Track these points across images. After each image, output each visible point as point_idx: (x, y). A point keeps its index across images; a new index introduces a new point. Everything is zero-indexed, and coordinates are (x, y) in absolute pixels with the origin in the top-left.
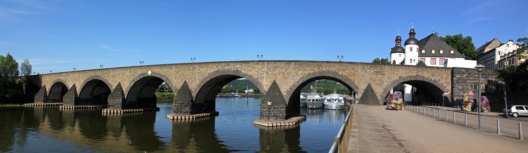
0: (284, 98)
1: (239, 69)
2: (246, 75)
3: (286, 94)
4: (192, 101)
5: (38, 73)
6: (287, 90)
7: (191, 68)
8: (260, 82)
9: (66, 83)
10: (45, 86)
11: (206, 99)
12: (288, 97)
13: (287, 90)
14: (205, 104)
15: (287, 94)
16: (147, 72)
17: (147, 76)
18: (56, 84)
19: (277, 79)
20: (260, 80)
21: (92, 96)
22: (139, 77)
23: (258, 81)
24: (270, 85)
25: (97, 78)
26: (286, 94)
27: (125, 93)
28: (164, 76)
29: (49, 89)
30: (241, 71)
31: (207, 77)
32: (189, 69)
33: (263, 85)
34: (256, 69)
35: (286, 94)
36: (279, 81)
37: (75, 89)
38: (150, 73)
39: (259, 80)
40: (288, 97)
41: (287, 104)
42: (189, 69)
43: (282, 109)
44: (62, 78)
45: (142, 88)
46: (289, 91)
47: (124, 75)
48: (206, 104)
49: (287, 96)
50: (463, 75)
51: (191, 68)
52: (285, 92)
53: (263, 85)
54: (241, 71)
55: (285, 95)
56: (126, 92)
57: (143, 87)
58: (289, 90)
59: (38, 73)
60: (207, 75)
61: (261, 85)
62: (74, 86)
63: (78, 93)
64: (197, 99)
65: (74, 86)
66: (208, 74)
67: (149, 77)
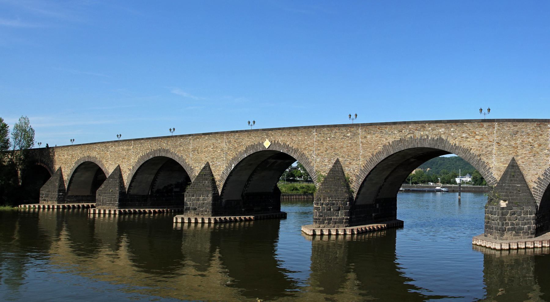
0: (533, 193)
1: (443, 137)
2: (457, 148)
3: (535, 185)
4: (351, 199)
5: (47, 144)
6: (539, 178)
7: (349, 135)
8: (484, 162)
9: (103, 165)
10: (61, 170)
11: (378, 195)
12: (540, 191)
13: (539, 178)
14: (376, 206)
15: (537, 186)
16: (263, 143)
17: (261, 149)
18: (82, 166)
19: (517, 156)
20: (484, 159)
21: (154, 190)
22: (245, 152)
23: (480, 159)
24: (504, 167)
25: (163, 154)
26: (536, 185)
27: (217, 183)
28: (296, 151)
29: (68, 175)
30: (447, 140)
31: (380, 152)
32: (344, 136)
33: (490, 168)
34: (476, 137)
35: (535, 185)
36: (523, 160)
37: (121, 177)
38: (267, 144)
39: (482, 157)
40: (540, 191)
41: (538, 205)
42: (344, 136)
43: (529, 216)
44: (94, 155)
45: (252, 174)
46: (542, 181)
47: (217, 147)
48: (378, 205)
49: (537, 190)
50: (545, 151)
51: (349, 135)
52: (535, 182)
53: (490, 168)
54: (447, 140)
55: (534, 188)
56: (220, 181)
57: (254, 171)
58: (542, 178)
59: (47, 144)
60: (380, 148)
61: (487, 168)
62: (118, 170)
63: (125, 184)
64: (360, 196)
65: (118, 170)
66: (382, 146)
67: (266, 152)
